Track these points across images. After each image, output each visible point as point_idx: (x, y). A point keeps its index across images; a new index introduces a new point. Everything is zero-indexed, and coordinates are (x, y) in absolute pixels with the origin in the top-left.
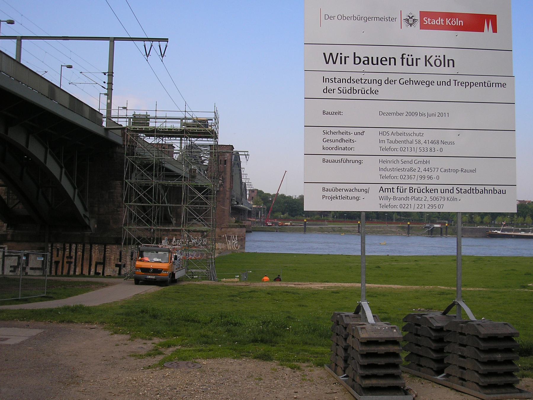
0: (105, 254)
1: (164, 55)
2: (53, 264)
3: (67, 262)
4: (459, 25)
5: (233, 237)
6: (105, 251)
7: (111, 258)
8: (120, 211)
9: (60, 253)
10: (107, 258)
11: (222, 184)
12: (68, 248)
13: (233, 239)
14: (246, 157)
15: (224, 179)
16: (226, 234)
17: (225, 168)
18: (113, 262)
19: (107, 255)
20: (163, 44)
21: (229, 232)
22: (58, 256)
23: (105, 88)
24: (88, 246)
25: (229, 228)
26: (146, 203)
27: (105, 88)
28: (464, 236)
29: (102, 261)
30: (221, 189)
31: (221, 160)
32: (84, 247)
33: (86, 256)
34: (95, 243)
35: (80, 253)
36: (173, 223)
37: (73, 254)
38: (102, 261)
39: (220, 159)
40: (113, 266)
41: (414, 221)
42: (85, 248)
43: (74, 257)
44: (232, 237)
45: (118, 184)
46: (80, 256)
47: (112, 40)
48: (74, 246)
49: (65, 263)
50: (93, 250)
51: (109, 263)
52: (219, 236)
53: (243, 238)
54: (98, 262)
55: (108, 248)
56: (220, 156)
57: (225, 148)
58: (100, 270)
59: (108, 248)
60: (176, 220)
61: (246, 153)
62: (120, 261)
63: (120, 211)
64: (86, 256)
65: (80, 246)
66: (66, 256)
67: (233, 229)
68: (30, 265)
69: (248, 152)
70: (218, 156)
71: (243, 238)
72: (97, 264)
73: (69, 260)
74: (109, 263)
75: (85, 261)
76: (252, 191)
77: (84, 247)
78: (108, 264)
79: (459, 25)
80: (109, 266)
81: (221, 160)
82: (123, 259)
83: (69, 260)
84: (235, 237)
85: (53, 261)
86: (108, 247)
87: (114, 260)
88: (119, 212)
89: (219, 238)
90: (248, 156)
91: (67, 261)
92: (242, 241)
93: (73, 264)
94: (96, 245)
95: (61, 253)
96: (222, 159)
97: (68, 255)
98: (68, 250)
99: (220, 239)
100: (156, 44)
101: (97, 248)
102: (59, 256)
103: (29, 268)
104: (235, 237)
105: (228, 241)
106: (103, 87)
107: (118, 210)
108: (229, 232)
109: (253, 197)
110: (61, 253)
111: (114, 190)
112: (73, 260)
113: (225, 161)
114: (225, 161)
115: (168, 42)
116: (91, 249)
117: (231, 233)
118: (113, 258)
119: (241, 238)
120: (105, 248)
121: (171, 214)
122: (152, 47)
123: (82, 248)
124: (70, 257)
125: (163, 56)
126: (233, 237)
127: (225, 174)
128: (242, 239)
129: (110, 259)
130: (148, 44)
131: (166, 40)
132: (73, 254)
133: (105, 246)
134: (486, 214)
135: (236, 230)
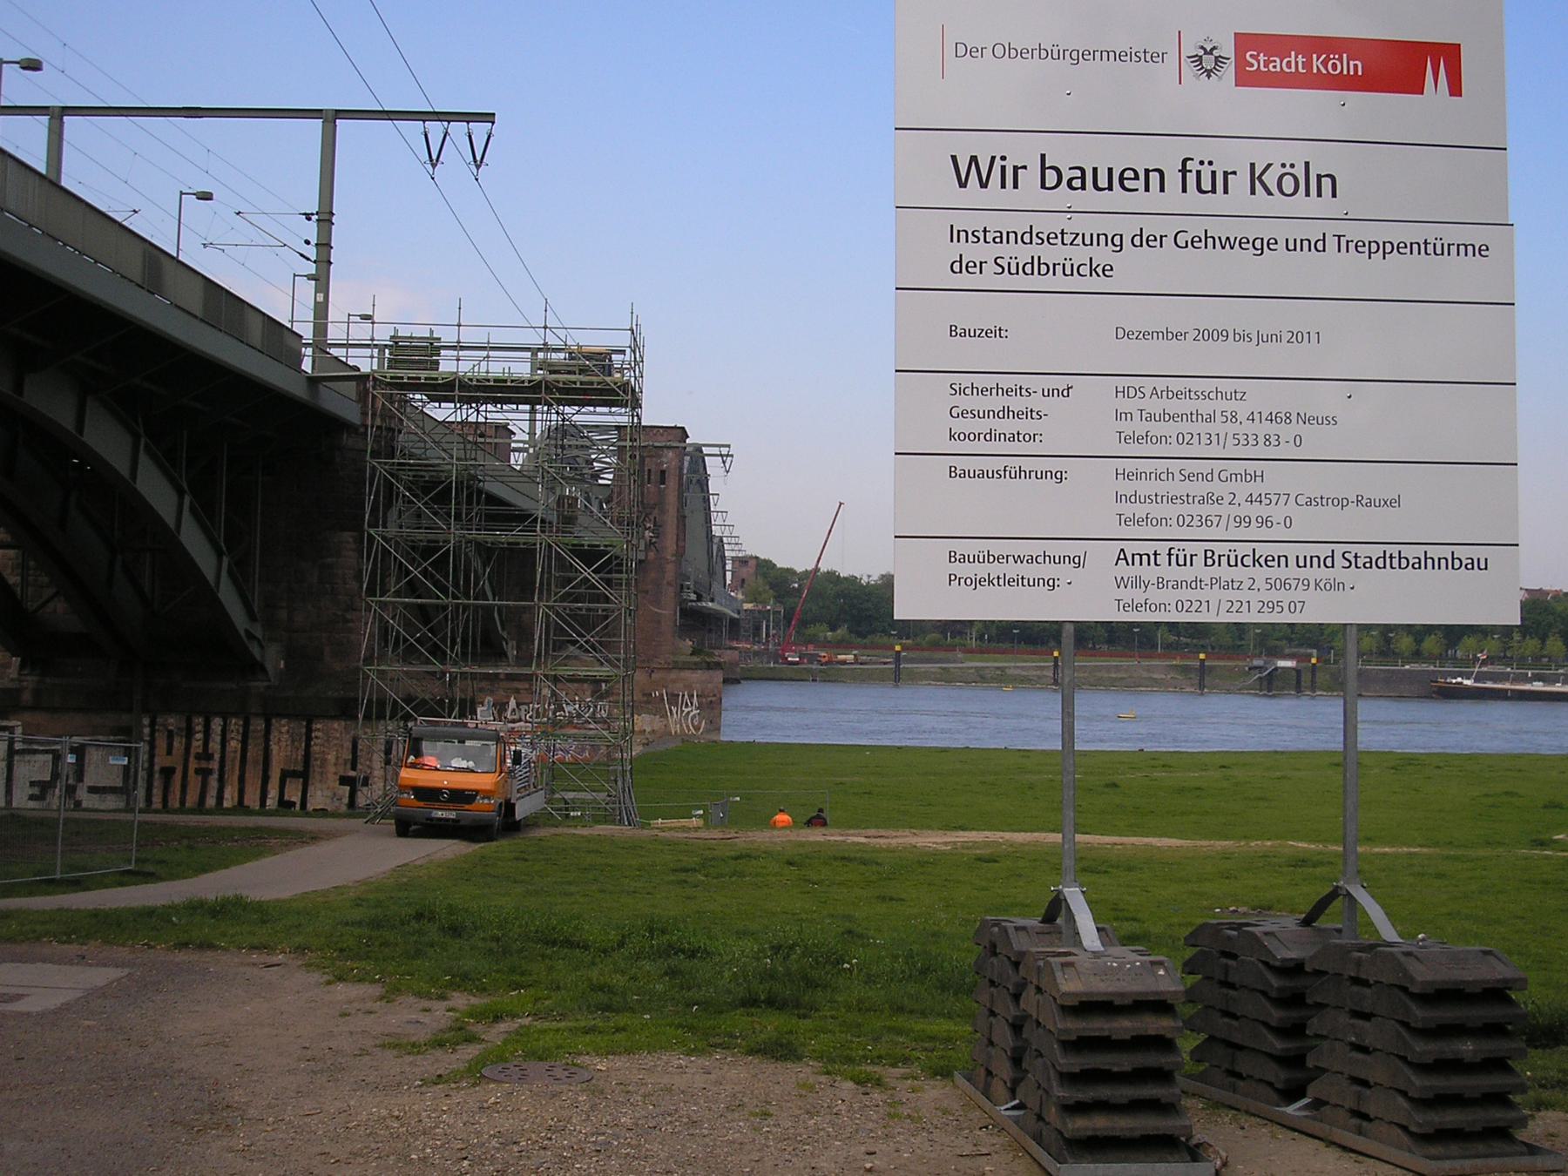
0: (308, 746)
1: (481, 162)
2: (157, 776)
3: (197, 771)
4: (1352, 73)
5: (686, 696)
6: (309, 739)
7: (326, 760)
8: (352, 621)
9: (176, 744)
10: (316, 760)
11: (654, 540)
12: (199, 728)
13: (687, 703)
14: (724, 462)
15: (660, 526)
16: (666, 687)
17: (661, 494)
18: (332, 769)
19: (315, 749)
20: (480, 129)
21: (674, 681)
22: (169, 752)
23: (308, 259)
24: (258, 725)
25: (674, 671)
26: (431, 598)
27: (308, 259)
28: (1364, 694)
29: (300, 768)
30: (652, 555)
31: (649, 470)
32: (246, 725)
33: (254, 751)
34: (280, 715)
35: (234, 744)
36: (509, 654)
37: (215, 746)
38: (300, 768)
39: (646, 469)
40: (333, 781)
41: (1217, 651)
42: (251, 728)
43: (217, 756)
44: (683, 696)
45: (348, 542)
46: (235, 752)
47: (331, 118)
48: (217, 725)
49: (191, 772)
50: (274, 735)
51: (322, 773)
52: (644, 695)
53: (714, 699)
54: (288, 771)
55: (319, 730)
56: (647, 460)
57: (662, 435)
58: (294, 795)
59: (319, 730)
60: (519, 648)
61: (724, 451)
62: (354, 768)
63: (352, 621)
64: (254, 751)
65: (235, 724)
66: (193, 751)
67: (687, 674)
68: (89, 780)
69: (729, 446)
70: (642, 459)
71: (714, 699)
72: (285, 775)
73: (204, 765)
74: (322, 773)
75: (249, 767)
76: (742, 562)
77: (246, 725)
78: (318, 777)
79: (1352, 73)
80: (321, 781)
81: (649, 470)
82: (361, 760)
83: (204, 765)
84: (691, 696)
85: (157, 768)
86: (319, 726)
87: (335, 764)
88: (351, 625)
89: (645, 699)
90: (729, 459)
91: (196, 766)
92: (713, 709)
93: (216, 776)
94: (284, 721)
95: (178, 744)
96: (653, 468)
97: (200, 750)
98: (199, 736)
99: (648, 702)
100: (459, 129)
101: (284, 729)
102: (174, 752)
103: (85, 789)
104: (691, 696)
105: (671, 710)
106: (302, 255)
107: (348, 616)
108: (674, 681)
109: (743, 581)
110: (178, 744)
111: (334, 560)
112: (215, 765)
113: (663, 472)
114: (663, 472)
115: (493, 123)
116: (268, 732)
117: (681, 685)
118: (331, 757)
119: (709, 699)
120: (309, 730)
121: (503, 629)
122: (448, 137)
123: (241, 730)
124: (206, 755)
125: (480, 166)
126: (686, 696)
127: (663, 512)
128: (711, 702)
129: (324, 761)
130: (435, 129)
131: (489, 117)
132: (215, 746)
133: (309, 723)
134: (1429, 629)
135: (694, 675)
